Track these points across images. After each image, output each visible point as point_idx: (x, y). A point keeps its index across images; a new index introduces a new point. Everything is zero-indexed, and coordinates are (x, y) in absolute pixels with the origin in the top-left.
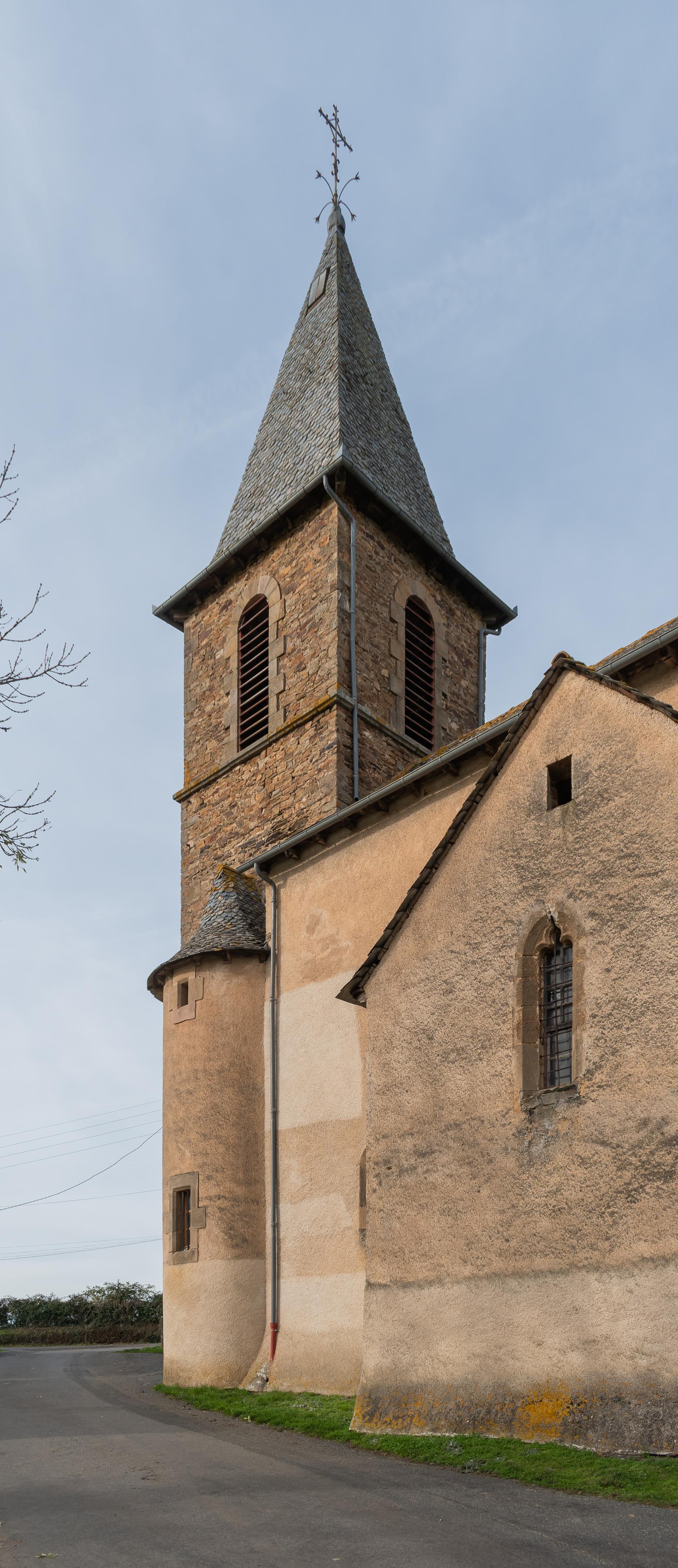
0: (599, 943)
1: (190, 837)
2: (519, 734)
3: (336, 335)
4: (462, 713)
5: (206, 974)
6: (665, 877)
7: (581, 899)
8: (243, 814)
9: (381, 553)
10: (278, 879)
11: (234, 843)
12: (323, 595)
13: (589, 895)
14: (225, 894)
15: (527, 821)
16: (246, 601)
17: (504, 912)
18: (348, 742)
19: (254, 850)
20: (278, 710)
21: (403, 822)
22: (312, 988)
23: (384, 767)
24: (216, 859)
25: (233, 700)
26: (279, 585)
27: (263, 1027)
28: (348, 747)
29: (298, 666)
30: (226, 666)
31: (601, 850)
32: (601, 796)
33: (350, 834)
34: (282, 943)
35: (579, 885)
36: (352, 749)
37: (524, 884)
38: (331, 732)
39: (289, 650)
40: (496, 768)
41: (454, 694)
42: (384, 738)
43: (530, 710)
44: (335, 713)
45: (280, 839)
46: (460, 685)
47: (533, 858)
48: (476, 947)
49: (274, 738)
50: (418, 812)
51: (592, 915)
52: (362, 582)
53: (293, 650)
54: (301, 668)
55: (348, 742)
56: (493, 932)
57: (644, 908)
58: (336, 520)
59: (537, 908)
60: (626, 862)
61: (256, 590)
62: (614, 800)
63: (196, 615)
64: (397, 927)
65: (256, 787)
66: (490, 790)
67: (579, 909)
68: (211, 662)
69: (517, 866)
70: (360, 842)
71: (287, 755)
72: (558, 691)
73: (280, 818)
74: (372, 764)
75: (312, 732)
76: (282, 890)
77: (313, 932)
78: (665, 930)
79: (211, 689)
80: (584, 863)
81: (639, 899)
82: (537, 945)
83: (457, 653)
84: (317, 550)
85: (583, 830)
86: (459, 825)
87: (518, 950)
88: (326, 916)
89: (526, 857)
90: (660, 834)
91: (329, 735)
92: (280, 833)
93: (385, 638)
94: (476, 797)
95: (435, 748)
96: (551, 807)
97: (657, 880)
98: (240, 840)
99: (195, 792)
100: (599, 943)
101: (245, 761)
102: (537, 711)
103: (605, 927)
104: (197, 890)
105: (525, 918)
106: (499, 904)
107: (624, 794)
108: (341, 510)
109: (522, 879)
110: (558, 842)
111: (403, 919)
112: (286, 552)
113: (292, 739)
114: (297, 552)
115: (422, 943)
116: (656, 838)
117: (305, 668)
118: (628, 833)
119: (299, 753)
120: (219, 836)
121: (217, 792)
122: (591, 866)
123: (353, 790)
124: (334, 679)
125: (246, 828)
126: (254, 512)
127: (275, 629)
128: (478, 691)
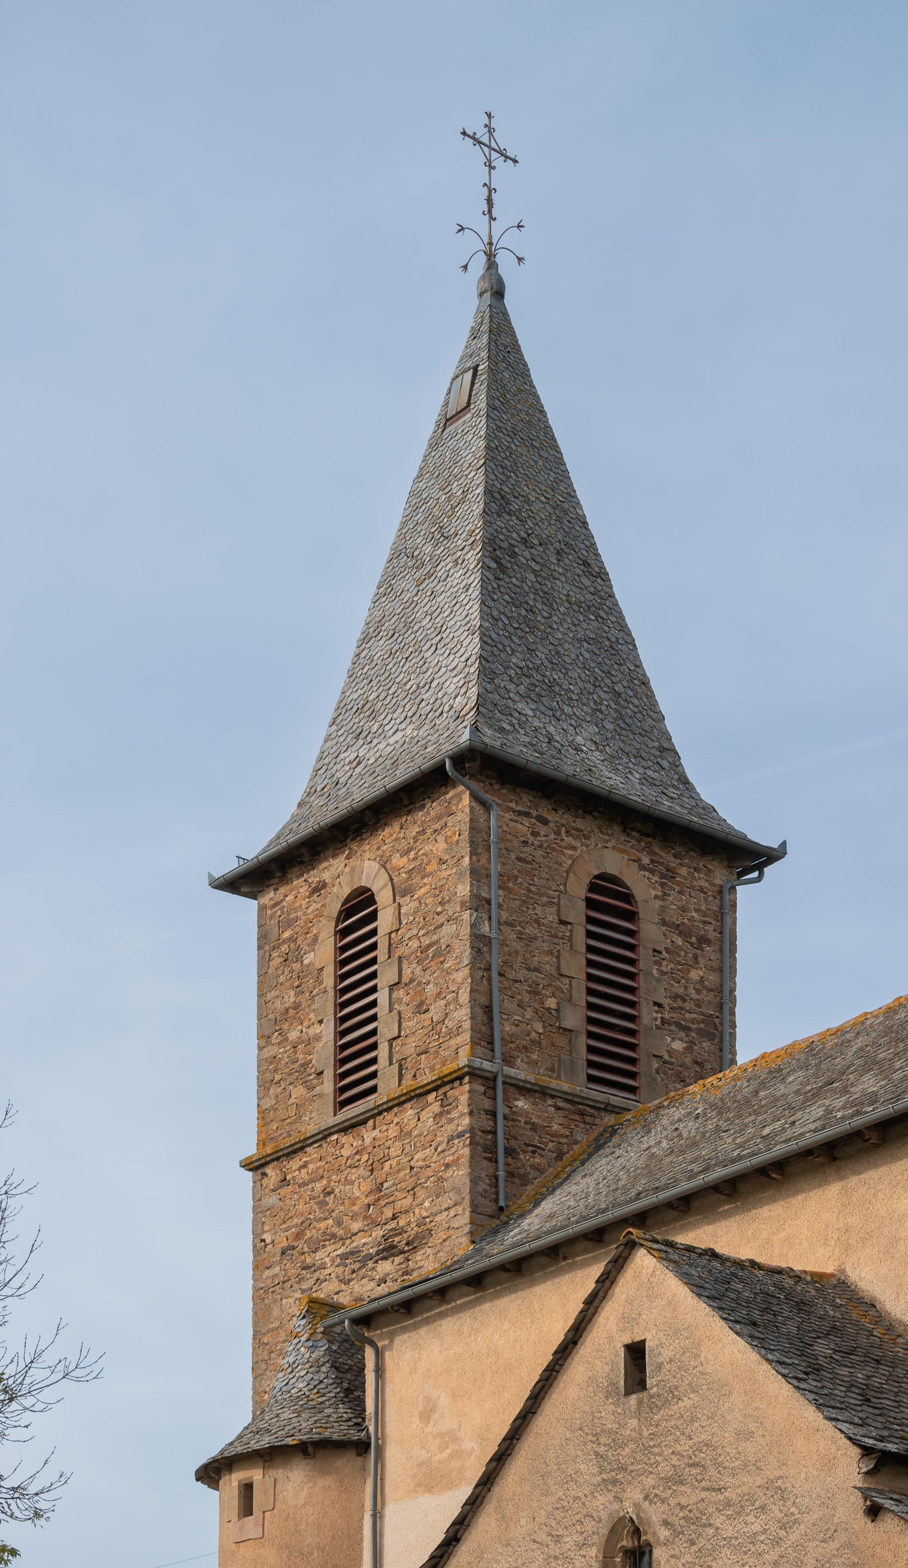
0: (672, 1556)
1: (266, 1228)
2: (595, 1304)
3: (480, 490)
4: (693, 1021)
5: (279, 1473)
6: (727, 1494)
7: (655, 1503)
8: (342, 1208)
9: (543, 830)
10: (381, 1338)
11: (330, 1249)
12: (450, 913)
13: (663, 1501)
14: (310, 1343)
15: (605, 1404)
16: (346, 891)
17: (584, 1504)
18: (487, 1124)
19: (358, 1265)
20: (391, 1064)
21: (539, 1289)
22: (427, 1501)
23: (551, 1145)
24: (304, 1269)
25: (328, 1031)
26: (391, 880)
27: (361, 1551)
28: (490, 1132)
29: (418, 1006)
30: (319, 980)
31: (673, 1453)
32: (672, 1392)
33: (475, 1293)
34: (387, 1431)
35: (654, 1488)
36: (494, 1133)
37: (603, 1475)
38: (462, 1115)
39: (405, 979)
40: (574, 1337)
41: (676, 997)
42: (550, 1102)
43: (604, 1281)
44: (467, 1087)
45: (393, 1255)
46: (687, 980)
47: (611, 1448)
48: (558, 1539)
49: (385, 1106)
50: (556, 1280)
51: (666, 1523)
52: (510, 885)
53: (412, 981)
54: (421, 1008)
55: (487, 1124)
56: (574, 1525)
57: (710, 1525)
58: (467, 810)
59: (615, 1506)
60: (694, 1471)
61: (360, 879)
62: (683, 1400)
63: (276, 890)
64: (478, 1502)
65: (361, 1171)
66: (569, 1359)
67: (654, 1514)
68: (296, 966)
69: (597, 1454)
70: (487, 1306)
71: (403, 1134)
72: (632, 1265)
73: (393, 1225)
74: (528, 1145)
75: (436, 1108)
76: (387, 1354)
77: (429, 1422)
78: (728, 1553)
79: (297, 1006)
80: (657, 1463)
81: (705, 1514)
82: (619, 1546)
83: (680, 934)
84: (442, 845)
85: (657, 1426)
86: (538, 1394)
87: (599, 1551)
88: (444, 1401)
89: (605, 1445)
90: (723, 1447)
91: (459, 1118)
92: (394, 1247)
93: (550, 952)
94: (554, 1366)
95: (643, 1092)
96: (628, 1393)
97: (721, 1497)
98: (338, 1245)
99: (273, 1160)
100: (672, 1556)
101: (347, 1128)
102: (613, 1282)
103: (677, 1540)
104: (276, 1311)
105: (604, 1515)
106: (580, 1494)
107: (692, 1396)
108: (474, 796)
109: (602, 1470)
110: (634, 1434)
111: (483, 1494)
112: (402, 835)
113: (409, 1112)
114: (415, 839)
115: (505, 1525)
116: (719, 1451)
117: (427, 1011)
118: (695, 1440)
119: (420, 1135)
120: (308, 1234)
121: (304, 1166)
122: (665, 1469)
123: (497, 1193)
124: (466, 1037)
125: (347, 1229)
126: (361, 742)
127: (387, 944)
128: (722, 979)
